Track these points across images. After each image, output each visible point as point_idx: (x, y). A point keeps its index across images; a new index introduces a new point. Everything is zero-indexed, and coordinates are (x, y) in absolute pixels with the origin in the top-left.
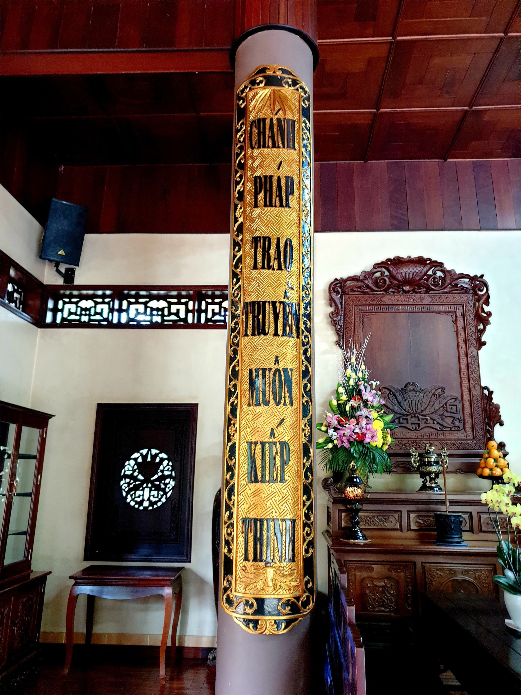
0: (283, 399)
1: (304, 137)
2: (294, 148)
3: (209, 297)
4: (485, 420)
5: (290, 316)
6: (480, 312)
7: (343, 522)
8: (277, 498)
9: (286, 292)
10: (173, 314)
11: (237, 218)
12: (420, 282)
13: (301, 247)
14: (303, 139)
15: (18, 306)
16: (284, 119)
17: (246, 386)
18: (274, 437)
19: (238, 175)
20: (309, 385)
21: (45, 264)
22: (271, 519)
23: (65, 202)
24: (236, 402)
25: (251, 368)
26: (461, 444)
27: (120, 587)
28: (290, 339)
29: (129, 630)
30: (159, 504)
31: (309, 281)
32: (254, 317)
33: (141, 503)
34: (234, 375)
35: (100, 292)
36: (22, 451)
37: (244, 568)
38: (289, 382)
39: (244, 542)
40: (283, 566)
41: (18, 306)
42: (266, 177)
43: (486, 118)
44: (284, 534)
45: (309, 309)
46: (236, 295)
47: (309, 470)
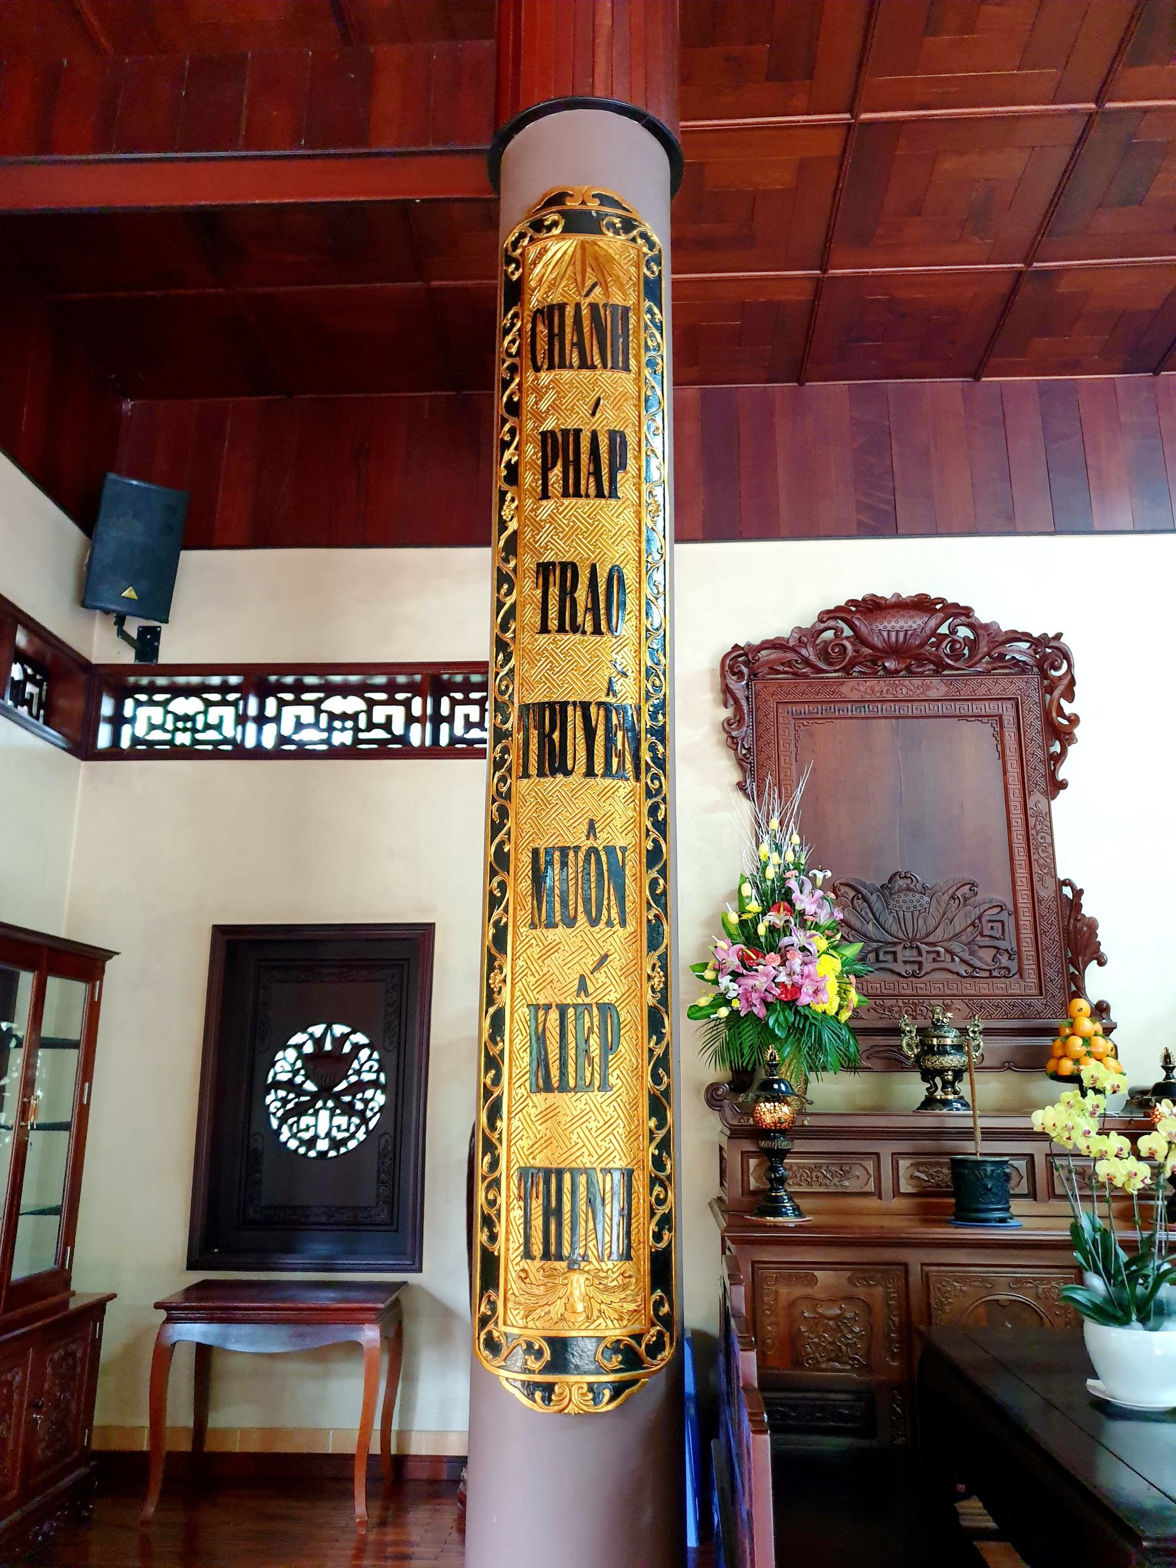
0: (605, 912)
1: (650, 343)
2: (627, 368)
3: (457, 688)
4: (1066, 952)
5: (620, 734)
6: (1054, 714)
7: (752, 1180)
8: (593, 1124)
9: (610, 682)
11: (506, 521)
12: (922, 651)
13: (644, 585)
14: (647, 348)
15: (34, 711)
16: (605, 305)
17: (526, 885)
19: (507, 427)
20: (661, 881)
21: (94, 617)
22: (579, 1169)
23: (135, 482)
24: (504, 920)
25: (537, 846)
26: (1030, 1005)
27: (266, 1326)
28: (621, 783)
29: (288, 1421)
30: (352, 1144)
31: (662, 658)
32: (542, 736)
33: (311, 1143)
34: (499, 862)
35: (216, 680)
36: (48, 1030)
37: (523, 1275)
38: (618, 873)
39: (522, 1220)
40: (605, 1268)
41: (34, 711)
42: (565, 432)
43: (1063, 288)
44: (607, 1201)
45: (660, 717)
46: (503, 688)
47: (662, 1064)
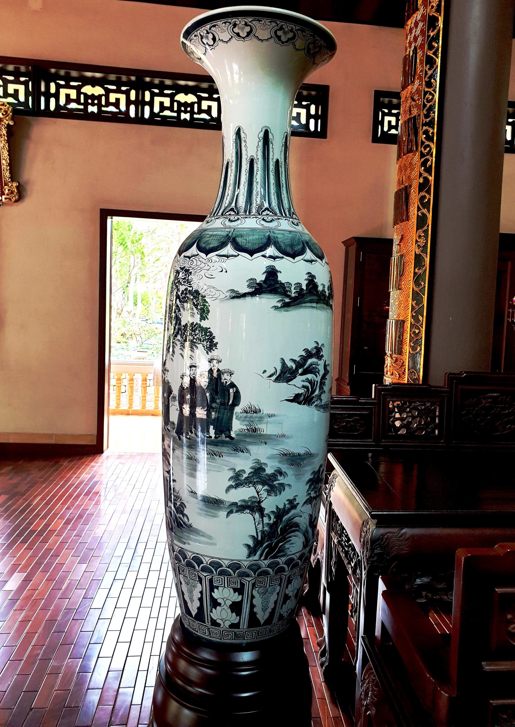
10: (112, 104)
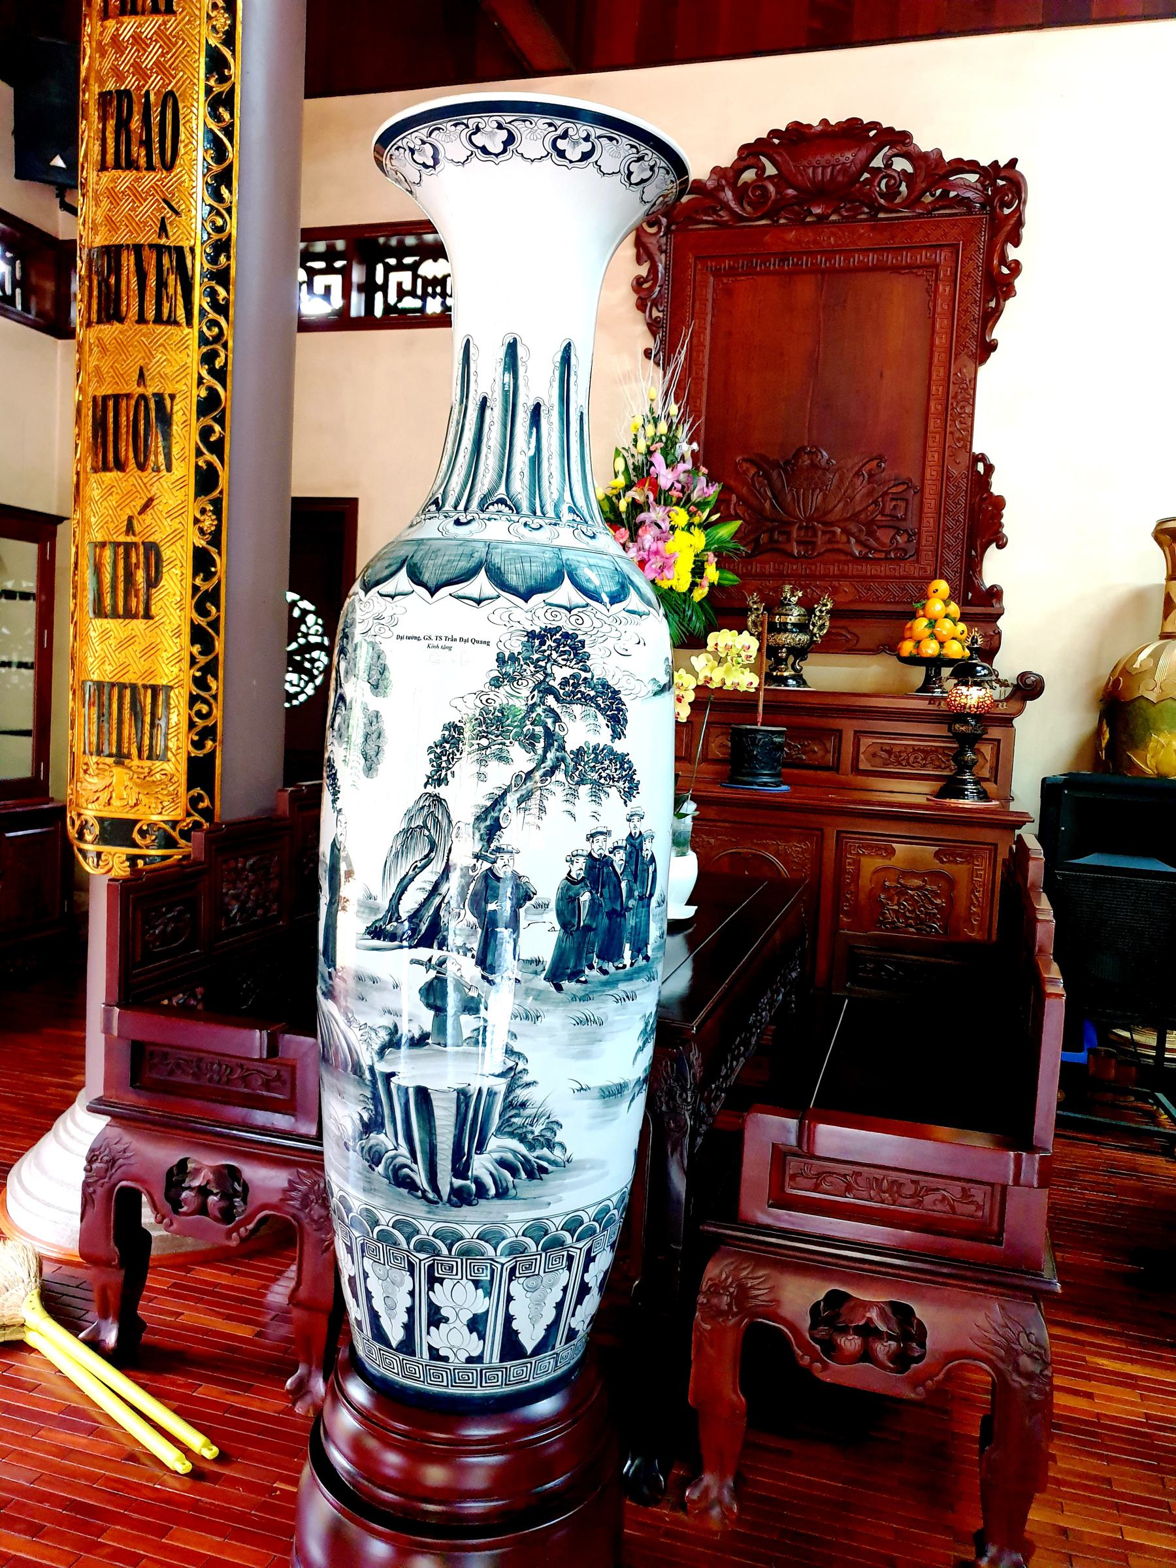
3: (392, 252)
18: (134, 535)
30: (302, 698)
38: (165, 419)
45: (223, 259)
